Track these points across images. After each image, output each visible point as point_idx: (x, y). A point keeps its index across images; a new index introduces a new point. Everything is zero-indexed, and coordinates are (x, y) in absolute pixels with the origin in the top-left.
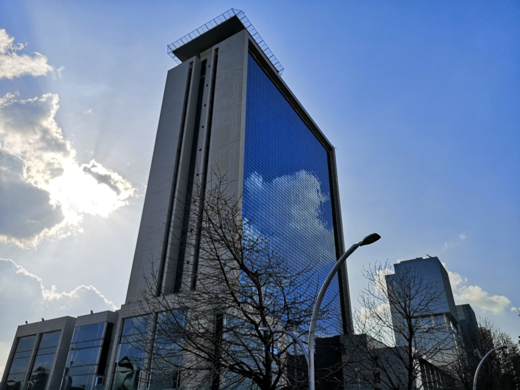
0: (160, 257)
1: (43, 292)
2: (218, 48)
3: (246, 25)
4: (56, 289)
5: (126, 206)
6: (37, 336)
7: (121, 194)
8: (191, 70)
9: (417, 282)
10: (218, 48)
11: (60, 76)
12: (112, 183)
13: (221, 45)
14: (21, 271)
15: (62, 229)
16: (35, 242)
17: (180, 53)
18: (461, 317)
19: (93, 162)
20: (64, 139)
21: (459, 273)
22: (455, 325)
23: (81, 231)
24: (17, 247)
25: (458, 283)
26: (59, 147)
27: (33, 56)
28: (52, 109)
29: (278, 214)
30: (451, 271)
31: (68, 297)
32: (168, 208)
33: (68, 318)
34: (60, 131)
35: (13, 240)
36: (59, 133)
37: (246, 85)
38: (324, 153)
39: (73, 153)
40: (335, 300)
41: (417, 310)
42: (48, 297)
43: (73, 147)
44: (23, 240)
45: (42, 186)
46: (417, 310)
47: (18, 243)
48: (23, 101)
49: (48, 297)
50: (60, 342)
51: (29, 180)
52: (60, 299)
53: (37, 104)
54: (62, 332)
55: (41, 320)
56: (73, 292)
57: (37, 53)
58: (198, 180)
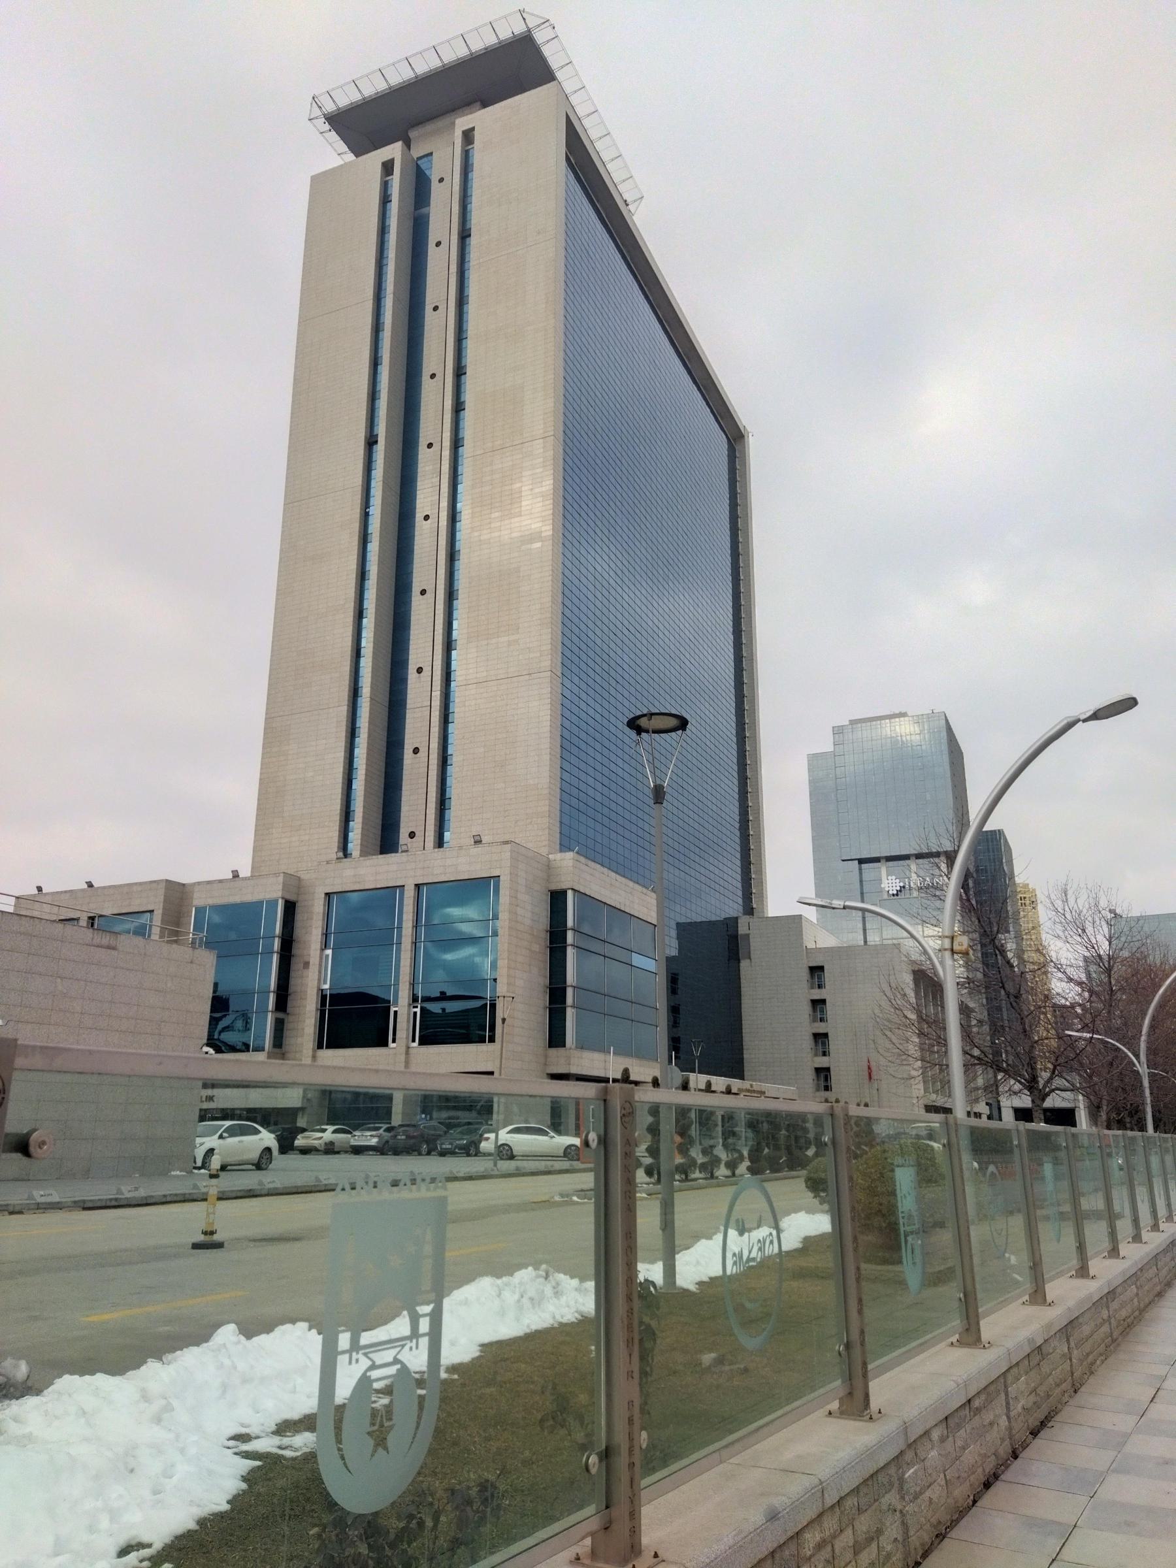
13: (480, 119)
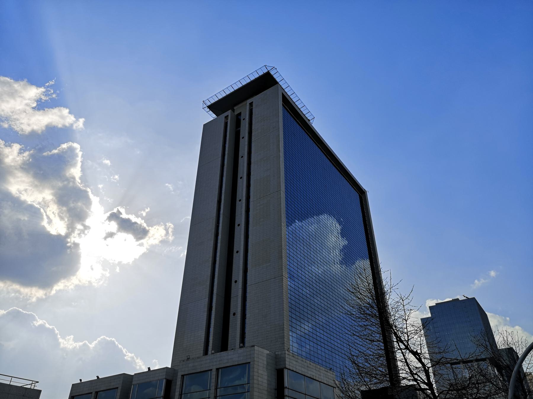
0: (206, 309)
3: (278, 80)
6: (93, 395)
8: (226, 124)
13: (255, 99)
17: (216, 107)
32: (211, 259)
33: (124, 376)
38: (355, 195)
54: (119, 390)
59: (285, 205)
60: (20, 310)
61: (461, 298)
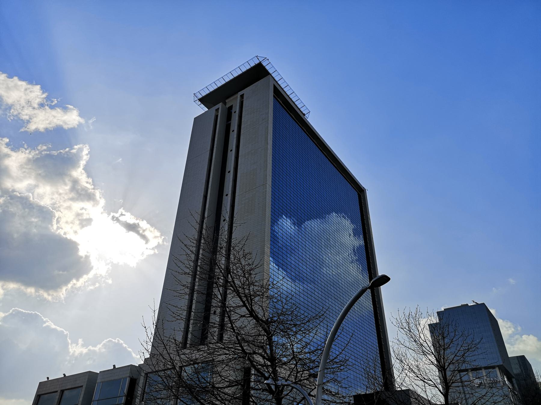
1: (70, 346)
2: (243, 94)
3: (271, 71)
4: (83, 343)
5: (155, 254)
6: (58, 393)
7: (149, 243)
8: (217, 117)
9: (451, 329)
10: (243, 94)
11: (91, 127)
12: (141, 232)
13: (246, 92)
14: (47, 324)
15: (89, 280)
16: (63, 292)
18: (516, 370)
19: (121, 210)
20: (94, 189)
21: (511, 322)
22: (509, 379)
23: (110, 282)
24: (45, 299)
25: (510, 332)
26: (89, 197)
27: (65, 109)
28: (82, 160)
29: (308, 260)
30: (501, 319)
31: (94, 351)
34: (90, 180)
35: (41, 292)
36: (90, 183)
37: (272, 129)
38: (354, 194)
39: (102, 202)
40: (346, 349)
41: (453, 361)
42: (75, 351)
43: (104, 195)
44: (51, 292)
45: (70, 236)
46: (453, 361)
47: (45, 295)
48: (55, 153)
49: (75, 351)
50: (81, 399)
51: (59, 231)
52: (87, 354)
53: (68, 155)
55: (63, 376)
56: (99, 346)
57: (69, 106)
58: (224, 226)
59: (270, 199)
60: (20, 310)
61: (471, 304)
